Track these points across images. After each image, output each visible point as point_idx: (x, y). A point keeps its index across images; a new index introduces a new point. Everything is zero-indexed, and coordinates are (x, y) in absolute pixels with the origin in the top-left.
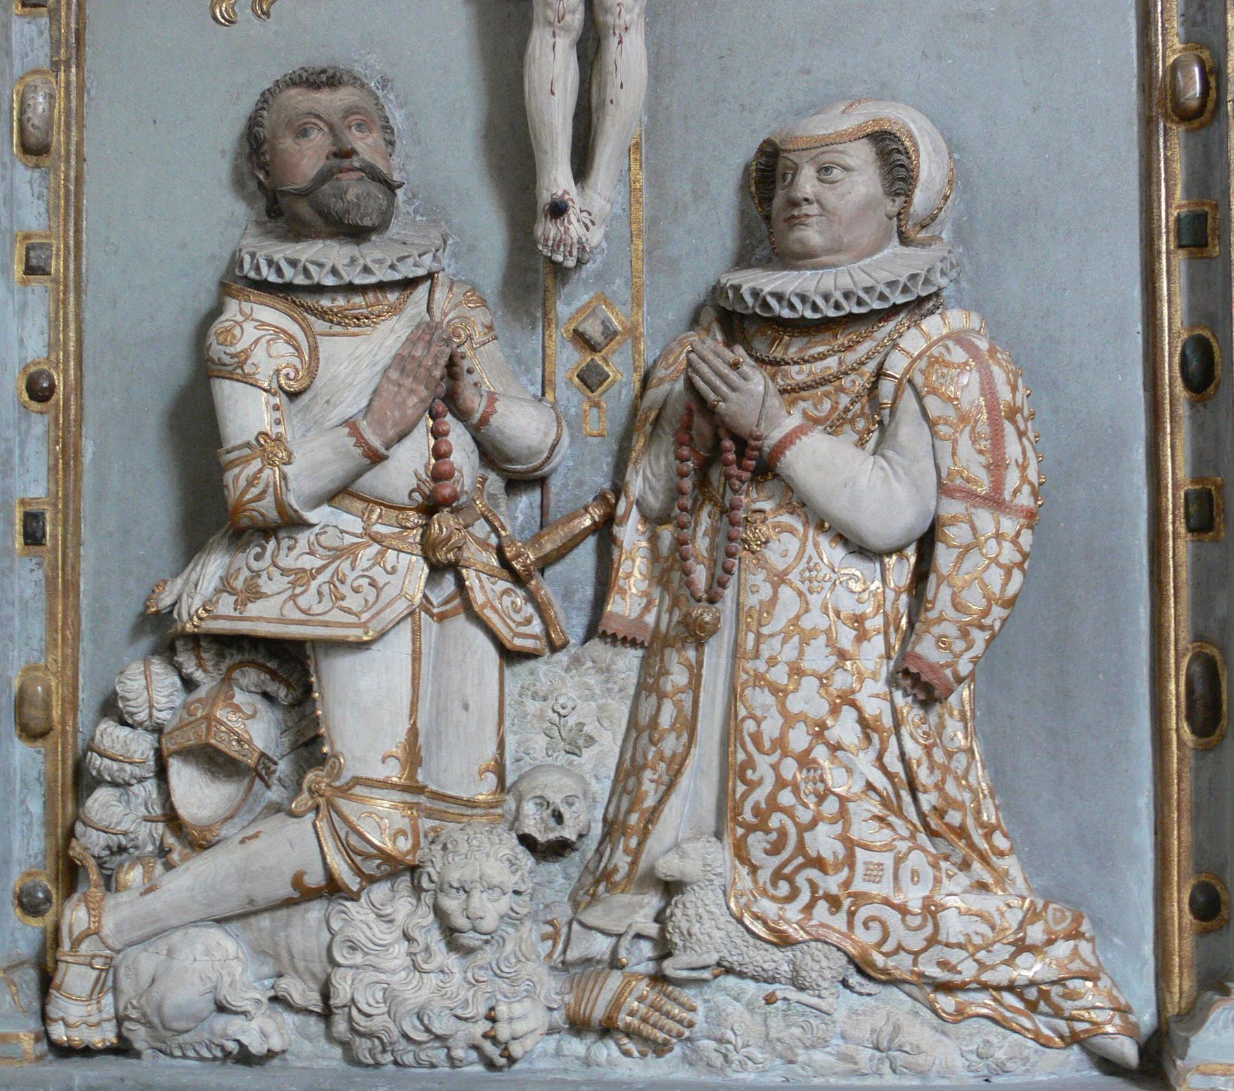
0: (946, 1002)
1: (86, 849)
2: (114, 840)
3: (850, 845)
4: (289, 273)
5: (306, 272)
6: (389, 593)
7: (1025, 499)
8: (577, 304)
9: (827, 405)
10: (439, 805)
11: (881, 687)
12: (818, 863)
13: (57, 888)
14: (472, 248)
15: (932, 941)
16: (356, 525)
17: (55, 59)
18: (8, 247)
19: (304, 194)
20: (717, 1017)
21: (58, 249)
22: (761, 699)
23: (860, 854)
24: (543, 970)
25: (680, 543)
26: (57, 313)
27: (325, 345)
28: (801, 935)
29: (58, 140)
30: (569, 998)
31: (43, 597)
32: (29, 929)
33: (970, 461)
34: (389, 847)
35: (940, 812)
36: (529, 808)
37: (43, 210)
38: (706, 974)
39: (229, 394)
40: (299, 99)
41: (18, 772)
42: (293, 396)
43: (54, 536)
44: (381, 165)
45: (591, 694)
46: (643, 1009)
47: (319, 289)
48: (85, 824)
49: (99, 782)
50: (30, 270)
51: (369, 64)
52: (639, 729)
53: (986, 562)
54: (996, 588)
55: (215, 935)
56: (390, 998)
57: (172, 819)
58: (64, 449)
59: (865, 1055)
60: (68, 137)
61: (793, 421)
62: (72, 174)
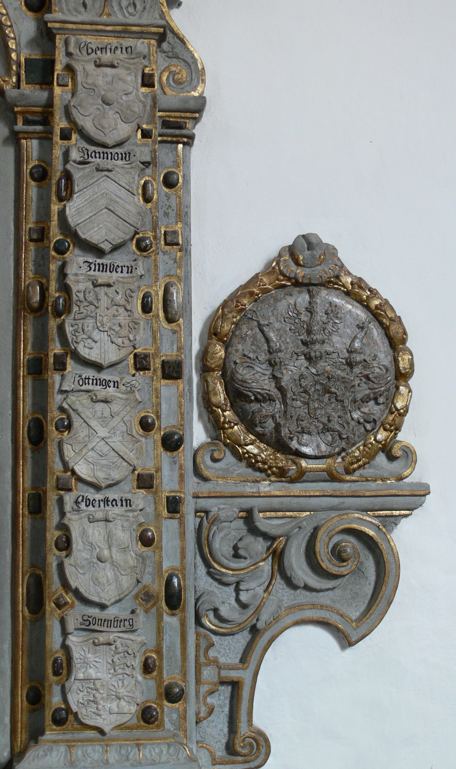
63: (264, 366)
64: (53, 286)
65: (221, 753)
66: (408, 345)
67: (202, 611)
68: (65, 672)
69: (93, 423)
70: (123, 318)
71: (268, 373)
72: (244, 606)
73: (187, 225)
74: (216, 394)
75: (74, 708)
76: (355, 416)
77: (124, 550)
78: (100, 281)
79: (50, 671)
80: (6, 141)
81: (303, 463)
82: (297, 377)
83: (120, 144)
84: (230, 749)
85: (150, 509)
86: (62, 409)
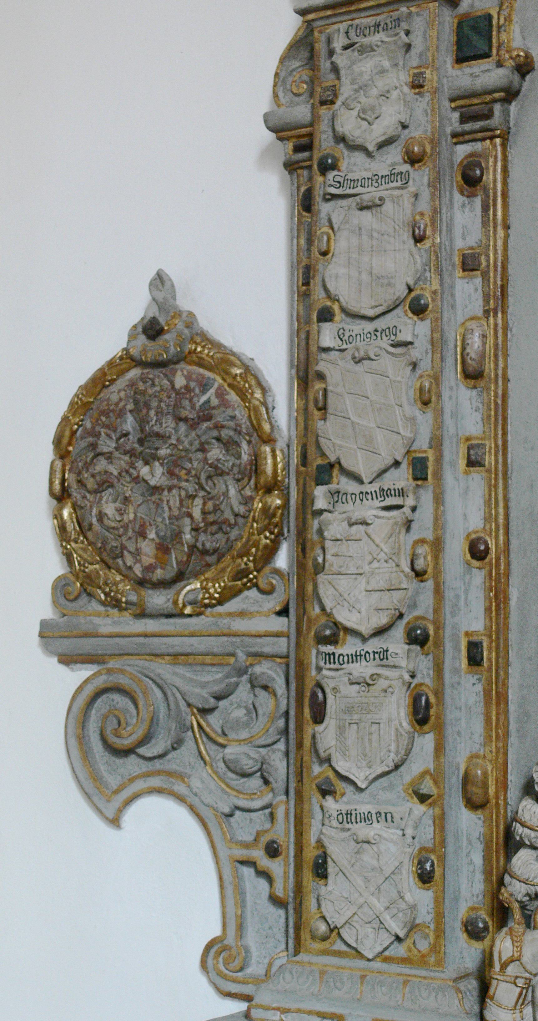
1: (511, 895)
13: (493, 920)
17: (487, 308)
18: (454, 446)
21: (490, 448)
26: (490, 495)
29: (489, 367)
31: (482, 704)
32: (473, 949)
37: (479, 419)
41: (465, 832)
43: (490, 660)
48: (511, 877)
49: (521, 845)
50: (471, 463)
58: (496, 595)
60: (496, 365)
62: (500, 392)
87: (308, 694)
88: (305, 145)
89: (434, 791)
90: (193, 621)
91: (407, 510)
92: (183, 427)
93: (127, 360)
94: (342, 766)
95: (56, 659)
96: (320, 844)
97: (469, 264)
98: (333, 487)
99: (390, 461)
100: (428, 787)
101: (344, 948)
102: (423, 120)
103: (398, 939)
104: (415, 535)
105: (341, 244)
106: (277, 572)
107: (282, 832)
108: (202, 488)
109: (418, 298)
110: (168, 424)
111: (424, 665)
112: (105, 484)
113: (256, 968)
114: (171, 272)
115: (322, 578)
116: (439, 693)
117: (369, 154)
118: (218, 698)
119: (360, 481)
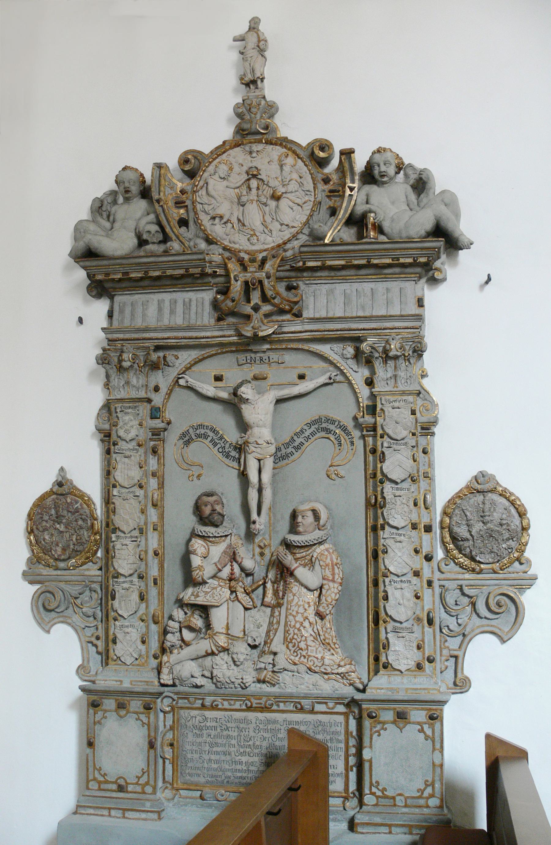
0: (326, 677)
2: (172, 644)
3: (307, 646)
4: (204, 533)
5: (207, 534)
6: (223, 596)
7: (339, 580)
8: (259, 540)
9: (303, 562)
10: (233, 638)
11: (313, 616)
12: (301, 649)
14: (239, 528)
15: (323, 664)
16: (217, 583)
19: (206, 518)
20: (284, 679)
22: (291, 618)
23: (309, 647)
24: (252, 670)
25: (277, 587)
27: (210, 547)
28: (298, 663)
29: (159, 503)
30: (257, 675)
33: (328, 573)
34: (223, 645)
35: (325, 640)
36: (249, 638)
38: (281, 670)
39: (193, 557)
40: (205, 499)
42: (205, 558)
44: (221, 512)
45: (262, 616)
46: (270, 677)
47: (209, 537)
49: (169, 632)
50: (154, 529)
51: (219, 490)
52: (271, 623)
53: (332, 592)
54: (333, 597)
55: (191, 662)
56: (224, 675)
57: (183, 640)
59: (311, 686)
61: (296, 565)
63: (465, 526)
64: (379, 497)
65: (451, 685)
66: (528, 516)
67: (442, 627)
68: (387, 648)
69: (396, 551)
70: (406, 509)
71: (467, 529)
72: (460, 625)
73: (434, 469)
74: (446, 538)
75: (390, 662)
76: (503, 546)
77: (409, 600)
78: (396, 495)
79: (381, 647)
80: (360, 438)
81: (482, 566)
82: (478, 531)
83: (403, 439)
84: (455, 684)
85: (419, 585)
86: (384, 545)
87: (110, 593)
88: (108, 435)
89: (146, 619)
90: (73, 571)
91: (138, 542)
92: (70, 514)
93: (51, 492)
94: (120, 612)
95: (27, 582)
96: (114, 634)
97: (154, 475)
98: (117, 534)
99: (133, 528)
100: (144, 617)
101: (121, 663)
102: (142, 434)
103: (136, 659)
104: (140, 549)
105: (119, 466)
106: (98, 557)
107: (101, 632)
108: (76, 532)
109: (140, 484)
110: (65, 513)
111: (143, 584)
112: (45, 529)
113: (93, 672)
114: (64, 467)
115: (114, 560)
116: (147, 592)
117: (127, 442)
118: (80, 594)
119: (125, 533)
